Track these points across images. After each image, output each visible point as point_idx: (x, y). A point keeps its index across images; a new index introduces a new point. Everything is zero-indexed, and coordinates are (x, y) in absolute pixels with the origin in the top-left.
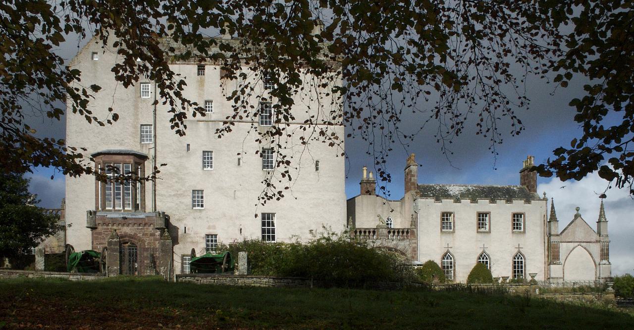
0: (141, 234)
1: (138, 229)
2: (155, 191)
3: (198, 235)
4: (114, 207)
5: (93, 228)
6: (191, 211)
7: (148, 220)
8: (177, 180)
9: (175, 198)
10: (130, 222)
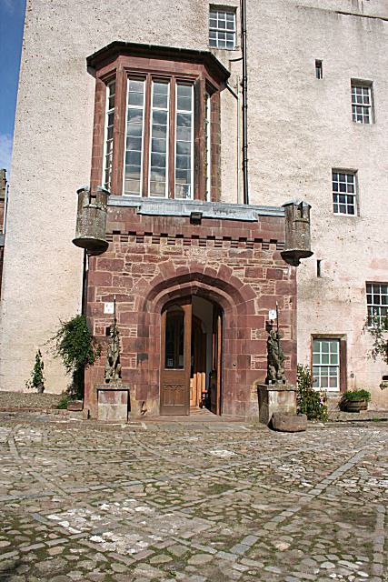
0: (243, 272)
1: (232, 255)
2: (245, 161)
3: (350, 283)
4: (145, 194)
5: (93, 247)
6: (332, 220)
7: (263, 228)
8: (296, 140)
9: (294, 185)
10: (213, 231)
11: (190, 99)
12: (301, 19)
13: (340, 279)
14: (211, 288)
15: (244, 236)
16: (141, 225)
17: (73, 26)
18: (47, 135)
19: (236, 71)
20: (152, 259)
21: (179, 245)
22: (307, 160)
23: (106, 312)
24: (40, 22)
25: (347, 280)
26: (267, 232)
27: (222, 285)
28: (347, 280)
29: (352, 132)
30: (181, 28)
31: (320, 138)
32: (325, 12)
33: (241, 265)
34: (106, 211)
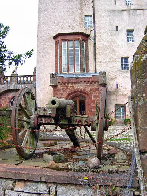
0: (89, 89)
1: (86, 85)
2: (95, 59)
5: (54, 87)
7: (94, 78)
8: (110, 51)
9: (109, 64)
10: (81, 80)
12: (111, 15)
13: (123, 88)
14: (82, 94)
15: (90, 81)
16: (64, 80)
17: (49, 28)
19: (92, 34)
20: (67, 88)
21: (74, 84)
26: (95, 79)
27: (84, 93)
29: (127, 46)
31: (117, 49)
32: (118, 11)
34: (56, 78)
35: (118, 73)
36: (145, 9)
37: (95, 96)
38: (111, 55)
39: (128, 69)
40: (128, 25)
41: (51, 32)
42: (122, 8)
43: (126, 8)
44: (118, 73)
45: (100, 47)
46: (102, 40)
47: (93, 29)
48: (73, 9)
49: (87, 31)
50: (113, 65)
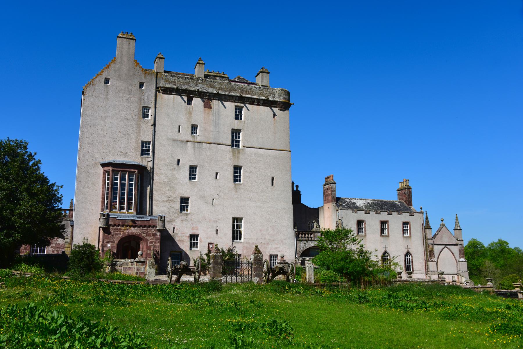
0: (145, 234)
3: (184, 235)
7: (152, 222)
8: (169, 188)
9: (167, 203)
11: (132, 198)
13: (181, 233)
17: (95, 151)
18: (87, 189)
20: (120, 231)
22: (172, 195)
23: (108, 246)
24: (84, 150)
25: (183, 234)
28: (183, 234)
29: (188, 184)
30: (131, 150)
31: (177, 187)
32: (182, 141)
33: (145, 232)
35: (176, 215)
36: (212, 143)
37: (151, 242)
38: (170, 193)
39: (188, 211)
40: (192, 160)
41: (98, 156)
42: (186, 137)
43: (190, 138)
44: (176, 215)
45: (157, 182)
46: (161, 174)
47: (151, 159)
48: (128, 130)
49: (144, 160)
50: (171, 205)
